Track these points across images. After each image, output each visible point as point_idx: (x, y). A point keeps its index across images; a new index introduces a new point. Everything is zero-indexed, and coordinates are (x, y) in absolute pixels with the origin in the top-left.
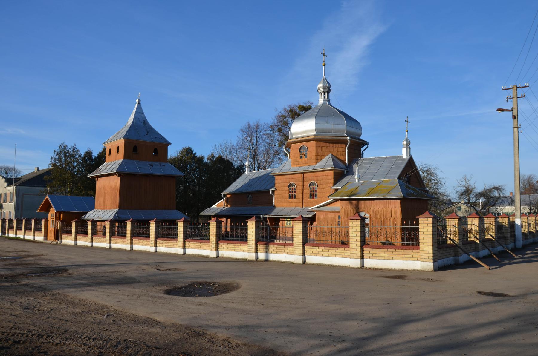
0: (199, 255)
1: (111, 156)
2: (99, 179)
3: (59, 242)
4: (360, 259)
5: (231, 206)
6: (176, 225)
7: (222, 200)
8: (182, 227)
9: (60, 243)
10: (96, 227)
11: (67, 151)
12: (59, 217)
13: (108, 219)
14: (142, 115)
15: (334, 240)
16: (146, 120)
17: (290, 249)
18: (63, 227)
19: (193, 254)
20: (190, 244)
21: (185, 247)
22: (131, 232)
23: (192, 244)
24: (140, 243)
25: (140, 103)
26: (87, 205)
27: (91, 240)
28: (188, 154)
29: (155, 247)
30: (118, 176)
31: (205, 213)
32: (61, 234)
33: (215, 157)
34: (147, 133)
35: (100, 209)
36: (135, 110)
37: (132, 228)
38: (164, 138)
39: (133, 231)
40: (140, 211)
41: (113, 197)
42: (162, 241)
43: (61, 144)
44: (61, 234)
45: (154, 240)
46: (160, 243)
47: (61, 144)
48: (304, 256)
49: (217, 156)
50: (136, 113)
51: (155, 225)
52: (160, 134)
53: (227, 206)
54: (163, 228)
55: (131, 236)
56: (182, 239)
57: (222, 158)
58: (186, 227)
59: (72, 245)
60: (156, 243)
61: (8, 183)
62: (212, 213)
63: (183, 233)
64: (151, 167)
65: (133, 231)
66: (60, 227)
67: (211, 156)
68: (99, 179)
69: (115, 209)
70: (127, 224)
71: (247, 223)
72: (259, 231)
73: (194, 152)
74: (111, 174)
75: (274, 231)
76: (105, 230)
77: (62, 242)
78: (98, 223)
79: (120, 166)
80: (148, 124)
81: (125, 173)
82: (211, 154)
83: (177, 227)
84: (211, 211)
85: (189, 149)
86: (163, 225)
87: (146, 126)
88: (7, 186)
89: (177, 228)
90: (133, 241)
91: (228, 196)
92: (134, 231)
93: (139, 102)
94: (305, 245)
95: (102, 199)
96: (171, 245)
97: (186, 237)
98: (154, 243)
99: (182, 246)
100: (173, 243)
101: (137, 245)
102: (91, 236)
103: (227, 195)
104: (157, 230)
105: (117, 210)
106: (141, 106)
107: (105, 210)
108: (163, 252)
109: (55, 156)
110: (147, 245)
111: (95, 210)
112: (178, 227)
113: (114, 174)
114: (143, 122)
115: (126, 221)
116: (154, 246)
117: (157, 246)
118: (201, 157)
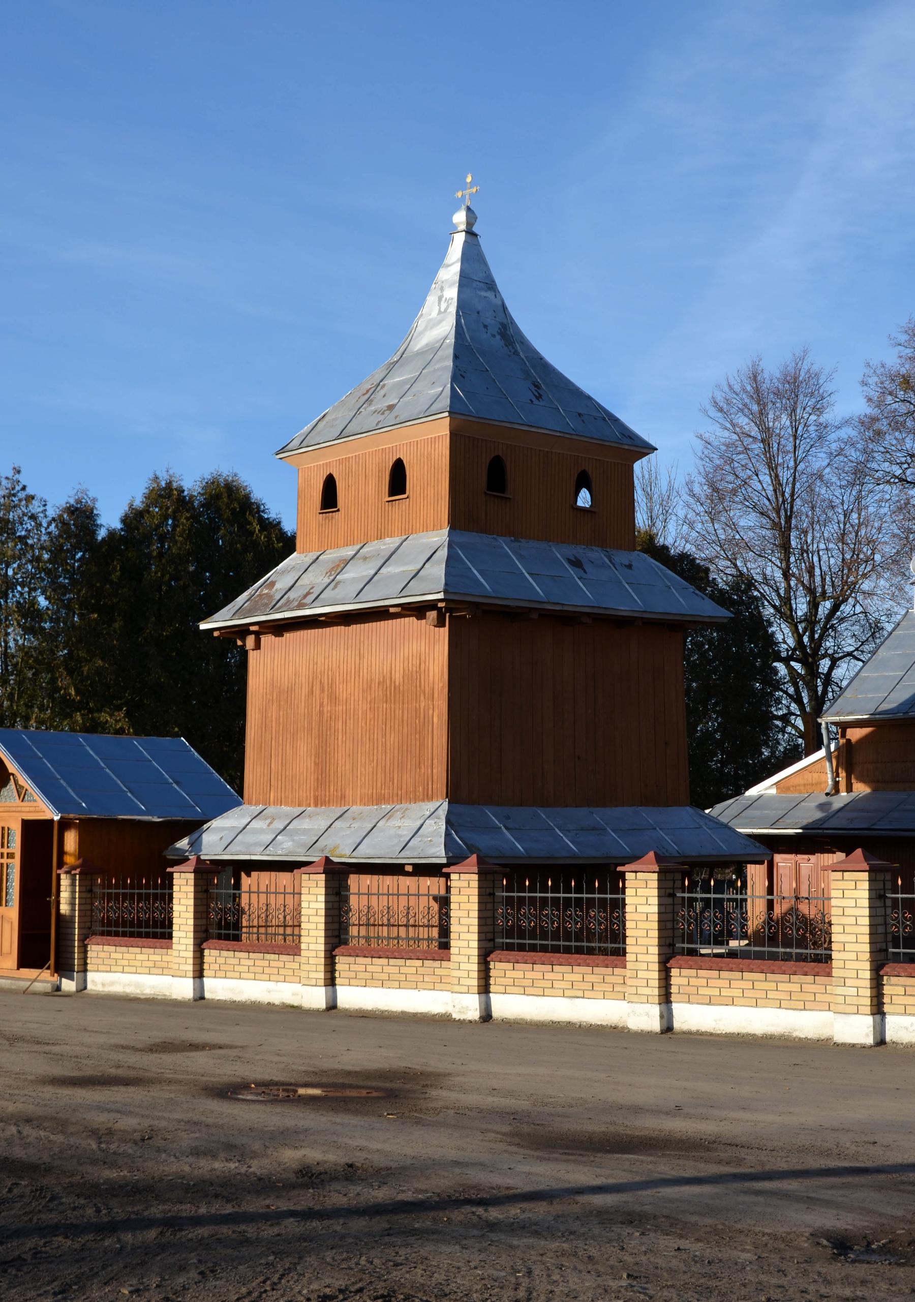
1: (404, 504)
3: (69, 985)
4: (660, 1004)
5: (875, 790)
6: (163, 886)
7: (822, 753)
9: (79, 991)
10: (346, 900)
13: (403, 854)
14: (490, 295)
15: (357, 935)
16: (513, 322)
17: (614, 975)
22: (660, 930)
25: (475, 229)
26: (177, 783)
32: (84, 939)
35: (292, 804)
36: (457, 268)
37: (330, 905)
40: (542, 813)
44: (84, 939)
48: (330, 988)
52: (589, 398)
53: (849, 789)
55: (194, 938)
59: (629, 1030)
66: (72, 904)
68: (266, 640)
70: (175, 882)
71: (172, 879)
72: (494, 910)
74: (392, 610)
75: (530, 910)
76: (449, 917)
77: (90, 986)
78: (354, 881)
80: (524, 342)
81: (477, 604)
83: (624, 900)
86: (110, 886)
87: (516, 353)
91: (855, 734)
94: (204, 944)
101: (710, 1004)
103: (849, 731)
106: (478, 245)
108: (269, 1004)
110: (160, 971)
112: (175, 895)
113: (418, 610)
114: (499, 334)
115: (619, 869)
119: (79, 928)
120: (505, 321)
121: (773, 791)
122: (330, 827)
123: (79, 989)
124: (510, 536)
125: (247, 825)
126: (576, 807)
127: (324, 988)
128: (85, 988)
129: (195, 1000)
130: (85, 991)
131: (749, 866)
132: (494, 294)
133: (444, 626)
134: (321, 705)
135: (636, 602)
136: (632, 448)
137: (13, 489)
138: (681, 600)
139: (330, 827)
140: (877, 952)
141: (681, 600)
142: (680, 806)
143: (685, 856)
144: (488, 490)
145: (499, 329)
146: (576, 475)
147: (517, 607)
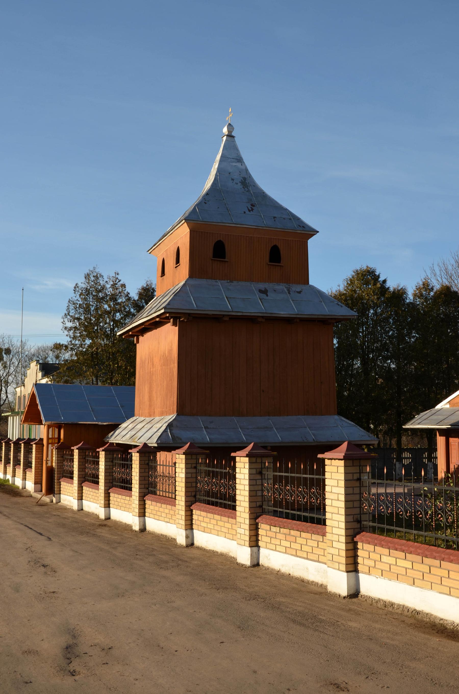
0: (418, 613)
2: (141, 338)
8: (342, 483)
11: (100, 287)
12: (56, 436)
14: (239, 165)
16: (250, 176)
18: (64, 461)
19: (392, 604)
20: (377, 557)
21: (356, 564)
23: (384, 559)
24: (210, 526)
25: (233, 134)
27: (105, 500)
28: (367, 283)
29: (251, 547)
30: (174, 324)
31: (419, 424)
33: (432, 289)
34: (249, 207)
38: (298, 219)
39: (194, 485)
40: (235, 419)
41: (165, 383)
42: (273, 529)
43: (90, 271)
44: (59, 479)
45: (247, 522)
46: (269, 533)
47: (90, 271)
49: (437, 287)
50: (221, 161)
51: (250, 469)
52: (286, 210)
54: (277, 480)
56: (343, 532)
57: (451, 292)
58: (359, 479)
60: (257, 535)
61: (44, 373)
62: (437, 424)
63: (347, 508)
64: (264, 296)
65: (194, 485)
66: (55, 463)
67: (422, 286)
69: (170, 414)
73: (381, 279)
79: (175, 295)
80: (255, 186)
81: (189, 314)
82: (421, 283)
84: (434, 417)
85: (368, 271)
87: (248, 191)
88: (42, 377)
89: (321, 485)
90: (195, 517)
92: (197, 483)
93: (228, 131)
95: (146, 389)
96: (305, 548)
97: (359, 521)
98: (247, 533)
99: (343, 560)
100: (310, 543)
102: (105, 490)
104: (260, 488)
105: (171, 417)
106: (234, 141)
107: (152, 418)
109: (77, 298)
111: (134, 418)
112: (327, 482)
114: (240, 182)
116: (247, 543)
117: (260, 543)
118: (399, 291)
119: (57, 474)
120: (246, 176)
121: (448, 406)
122: (143, 427)
123: (57, 502)
124: (227, 280)
125: (128, 426)
126: (261, 416)
127: (104, 509)
128: (60, 502)
129: (78, 510)
130: (59, 504)
131: (157, 453)
132: (240, 164)
133: (176, 326)
134: (150, 369)
135: (294, 309)
136: (303, 232)
137: (116, 281)
138: (325, 307)
139: (143, 427)
140: (257, 507)
141: (325, 307)
142: (330, 415)
143: (317, 442)
144: (270, 261)
145: (241, 180)
146: (270, 248)
147: (213, 315)
